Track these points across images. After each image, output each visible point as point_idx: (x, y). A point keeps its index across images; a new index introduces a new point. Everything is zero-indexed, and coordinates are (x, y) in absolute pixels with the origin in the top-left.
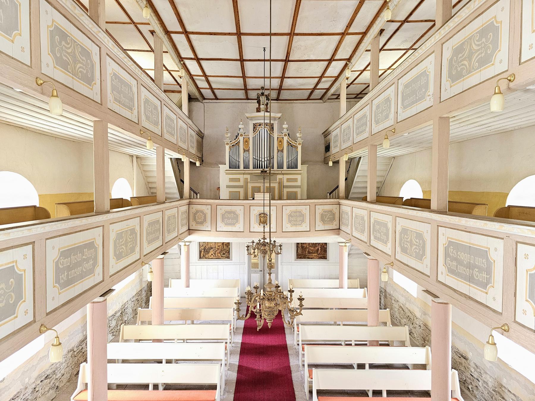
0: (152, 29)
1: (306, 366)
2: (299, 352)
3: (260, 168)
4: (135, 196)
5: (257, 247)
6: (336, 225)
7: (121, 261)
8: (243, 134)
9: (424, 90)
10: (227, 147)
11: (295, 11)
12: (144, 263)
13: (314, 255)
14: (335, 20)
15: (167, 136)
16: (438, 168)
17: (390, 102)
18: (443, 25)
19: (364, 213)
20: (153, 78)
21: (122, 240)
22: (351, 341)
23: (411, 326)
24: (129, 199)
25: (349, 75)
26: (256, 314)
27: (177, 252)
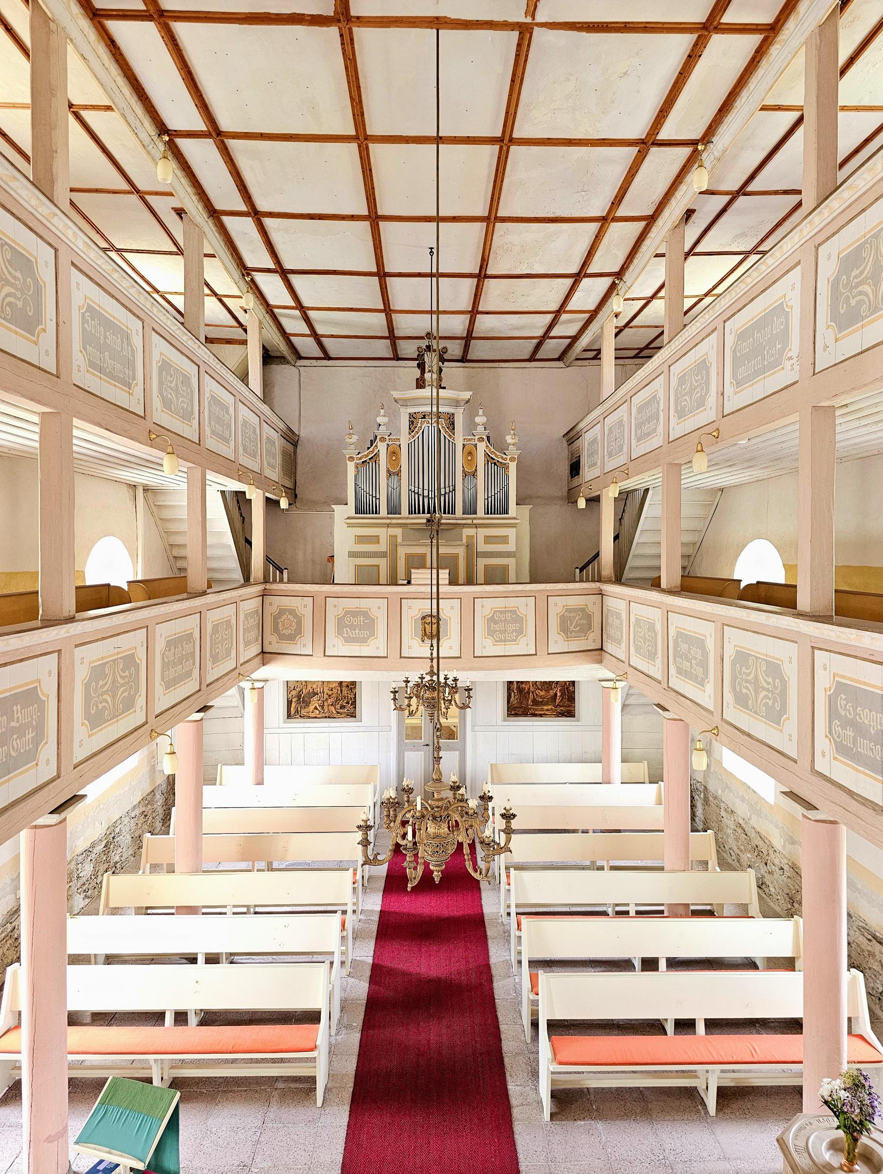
0: (178, 205)
1: (525, 964)
2: (509, 931)
3: (424, 512)
4: (139, 578)
5: (415, 692)
6: (594, 641)
7: (102, 729)
8: (386, 437)
9: (780, 346)
10: (351, 467)
11: (497, 170)
12: (156, 732)
13: (545, 708)
14: (585, 190)
15: (211, 443)
16: (812, 518)
17: (708, 369)
18: (818, 206)
19: (655, 615)
20: (183, 311)
21: (105, 682)
22: (628, 905)
23: (763, 870)
24: (125, 587)
25: (619, 307)
26: (404, 852)
27: (236, 704)
